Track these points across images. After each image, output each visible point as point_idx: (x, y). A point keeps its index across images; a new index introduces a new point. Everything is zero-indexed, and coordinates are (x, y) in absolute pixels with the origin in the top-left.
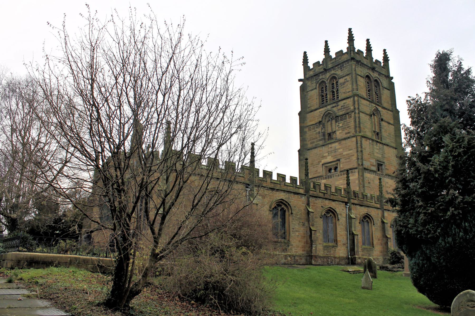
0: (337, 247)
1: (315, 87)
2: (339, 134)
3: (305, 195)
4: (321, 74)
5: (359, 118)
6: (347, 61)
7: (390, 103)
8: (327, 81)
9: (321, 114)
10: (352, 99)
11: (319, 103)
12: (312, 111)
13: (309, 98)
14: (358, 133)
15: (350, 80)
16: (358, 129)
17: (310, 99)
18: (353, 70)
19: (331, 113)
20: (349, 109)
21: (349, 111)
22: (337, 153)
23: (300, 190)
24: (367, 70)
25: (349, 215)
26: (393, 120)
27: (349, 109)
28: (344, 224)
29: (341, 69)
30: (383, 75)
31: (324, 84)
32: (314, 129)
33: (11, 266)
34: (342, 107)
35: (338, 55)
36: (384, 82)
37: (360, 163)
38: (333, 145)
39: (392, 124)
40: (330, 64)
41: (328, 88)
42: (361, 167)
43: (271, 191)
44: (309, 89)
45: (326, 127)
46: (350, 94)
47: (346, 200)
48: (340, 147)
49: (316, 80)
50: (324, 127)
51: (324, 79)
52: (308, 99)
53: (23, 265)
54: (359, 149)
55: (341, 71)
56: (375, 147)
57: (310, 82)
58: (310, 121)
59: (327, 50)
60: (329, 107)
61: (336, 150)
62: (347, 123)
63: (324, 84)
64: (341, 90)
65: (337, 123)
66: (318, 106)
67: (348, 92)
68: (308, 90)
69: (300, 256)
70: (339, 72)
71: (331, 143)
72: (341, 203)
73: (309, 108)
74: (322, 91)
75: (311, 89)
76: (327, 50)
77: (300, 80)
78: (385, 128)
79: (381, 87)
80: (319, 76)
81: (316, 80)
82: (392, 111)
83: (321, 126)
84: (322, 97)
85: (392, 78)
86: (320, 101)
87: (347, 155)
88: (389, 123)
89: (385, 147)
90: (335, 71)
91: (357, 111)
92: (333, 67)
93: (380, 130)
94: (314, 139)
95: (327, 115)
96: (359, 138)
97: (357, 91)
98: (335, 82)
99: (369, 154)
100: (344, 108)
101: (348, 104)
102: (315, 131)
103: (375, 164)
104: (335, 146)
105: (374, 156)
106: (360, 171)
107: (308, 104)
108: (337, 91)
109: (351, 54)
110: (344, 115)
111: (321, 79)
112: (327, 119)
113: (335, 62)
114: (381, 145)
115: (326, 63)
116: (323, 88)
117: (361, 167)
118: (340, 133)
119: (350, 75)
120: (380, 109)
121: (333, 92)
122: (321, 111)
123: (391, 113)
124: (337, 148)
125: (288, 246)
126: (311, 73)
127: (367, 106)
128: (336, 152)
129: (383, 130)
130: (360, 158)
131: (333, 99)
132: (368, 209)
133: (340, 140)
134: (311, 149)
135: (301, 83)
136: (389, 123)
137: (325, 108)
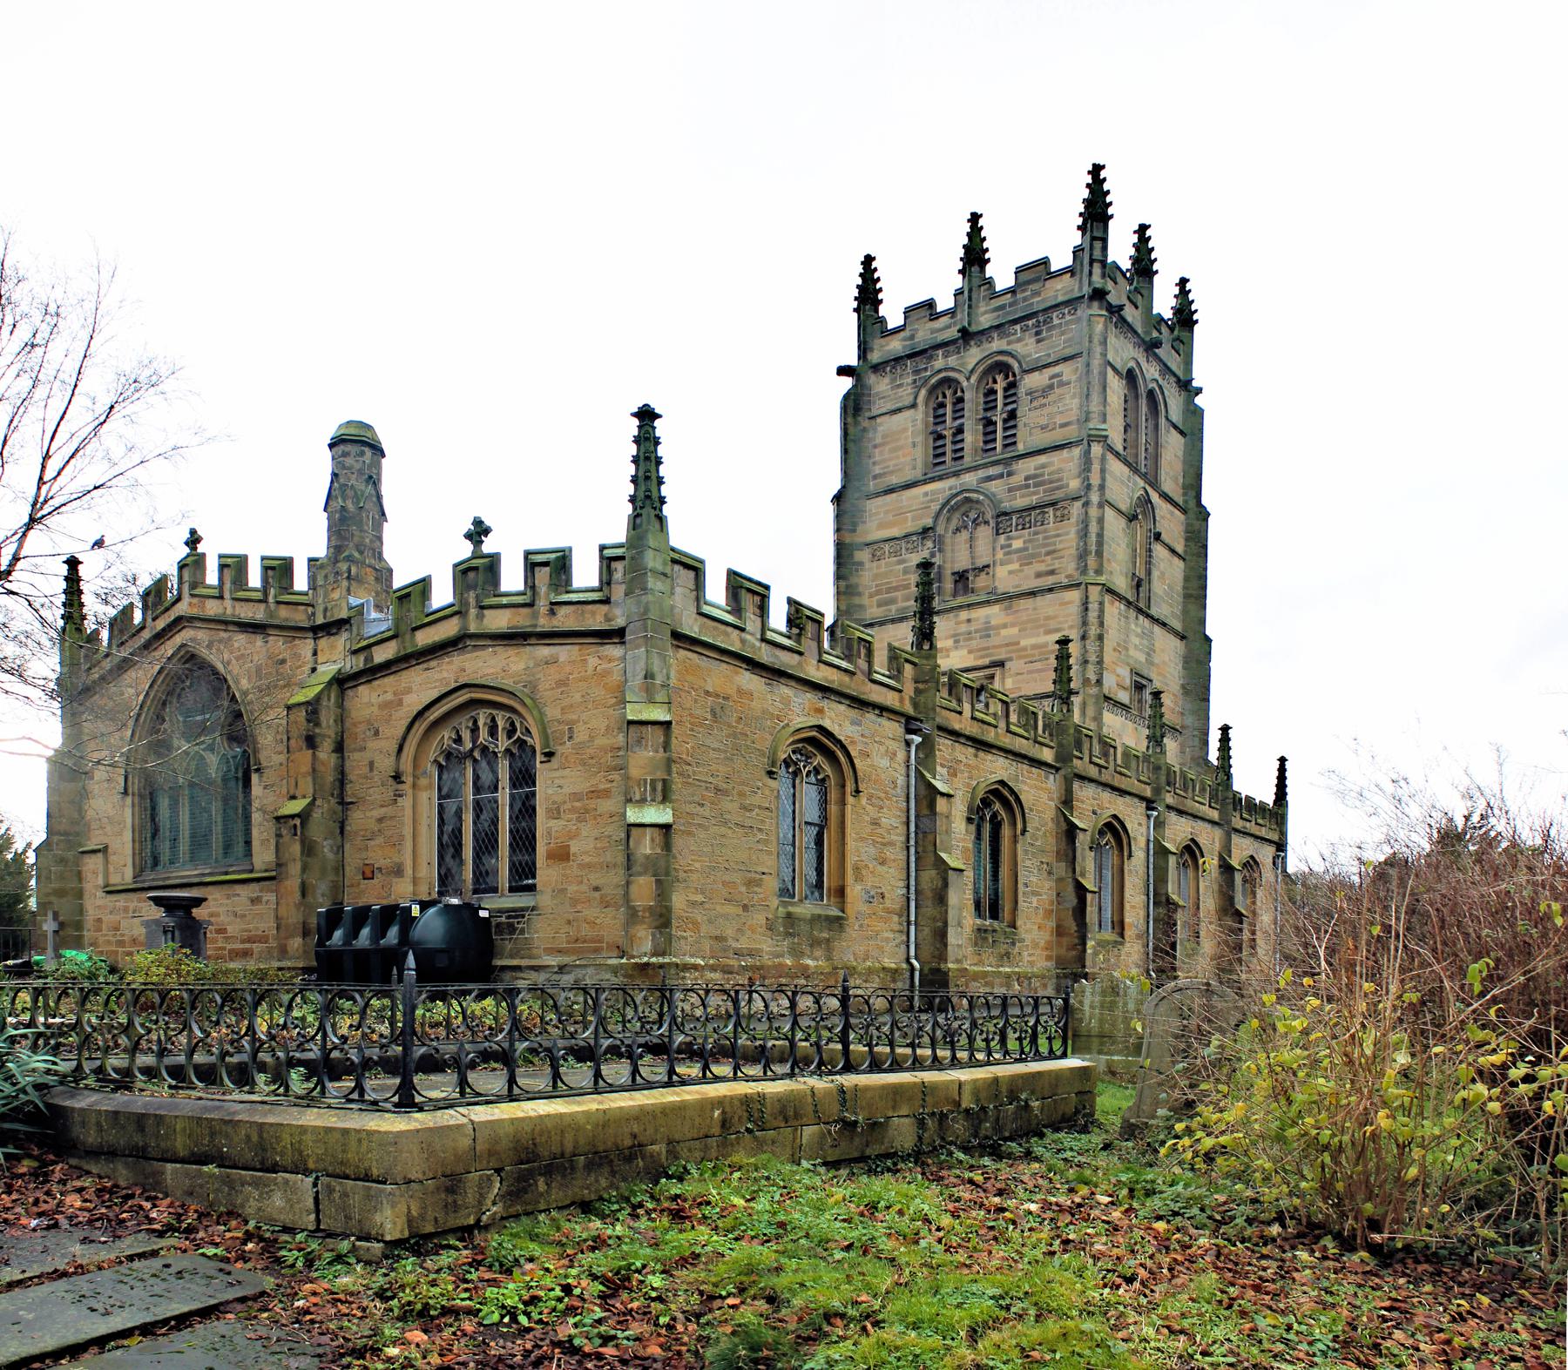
0: (1122, 944)
1: (908, 401)
2: (1005, 577)
3: (1057, 769)
4: (940, 352)
5: (1101, 520)
6: (1072, 303)
7: (1181, 480)
8: (968, 379)
9: (932, 501)
10: (1076, 452)
11: (926, 464)
12: (891, 491)
13: (878, 440)
14: (1091, 573)
15: (1074, 378)
16: (1092, 561)
17: (883, 444)
18: (1096, 340)
19: (978, 502)
20: (1058, 488)
21: (1059, 494)
22: (994, 641)
23: (1045, 750)
24: (1130, 346)
25: (1157, 841)
26: (1182, 542)
27: (1058, 488)
28: (1142, 870)
29: (1037, 333)
30: (1175, 375)
31: (948, 393)
32: (896, 553)
33: (410, 1221)
34: (1027, 478)
35: (1025, 276)
36: (1174, 403)
37: (1093, 678)
38: (980, 614)
39: (1179, 556)
40: (986, 312)
41: (967, 405)
42: (1094, 691)
43: (972, 750)
44: (878, 407)
45: (948, 548)
46: (1072, 433)
47: (1148, 792)
48: (1009, 619)
49: (916, 372)
50: (940, 550)
51: (953, 369)
52: (875, 447)
53: (480, 1203)
54: (1093, 631)
55: (1038, 341)
56: (1133, 626)
57: (887, 380)
58: (881, 526)
59: (974, 256)
60: (970, 479)
61: (987, 629)
62: (1046, 538)
63: (948, 393)
64: (1029, 417)
65: (1002, 537)
66: (918, 474)
67: (1063, 425)
68: (875, 412)
69: (1043, 977)
70: (1025, 347)
71: (969, 605)
72: (1136, 800)
73: (875, 477)
74: (935, 417)
75: (890, 406)
76: (974, 256)
77: (843, 371)
78: (1162, 566)
79: (1162, 421)
80: (931, 358)
81: (916, 372)
82: (1184, 511)
83: (930, 544)
84: (935, 440)
85: (1199, 391)
86: (926, 455)
87: (1034, 647)
88: (1173, 551)
89: (1157, 629)
90: (1009, 343)
91: (1095, 498)
92: (998, 327)
93: (1149, 573)
94: (896, 589)
95: (963, 508)
96: (1094, 592)
97: (1104, 421)
98: (1000, 387)
99: (1115, 650)
100: (1036, 485)
101: (1060, 471)
102: (903, 561)
103: (1127, 682)
104: (987, 616)
105: (1128, 656)
106: (1091, 702)
107: (874, 463)
108: (1012, 415)
109: (1090, 273)
110: (1034, 508)
111: (940, 371)
112: (954, 523)
113: (1011, 305)
114: (1147, 622)
115: (970, 307)
116: (943, 405)
117: (1094, 691)
118: (1010, 572)
119: (1079, 363)
120: (1155, 497)
121: (989, 423)
122: (934, 492)
123: (1182, 517)
124: (993, 623)
125: (1013, 944)
126: (896, 346)
127: (1122, 482)
128: (989, 636)
129: (1155, 574)
130: (1093, 658)
131: (987, 451)
132: (1194, 824)
133: (1011, 598)
134: (882, 623)
135: (847, 383)
136: (1173, 551)
137: (952, 482)
